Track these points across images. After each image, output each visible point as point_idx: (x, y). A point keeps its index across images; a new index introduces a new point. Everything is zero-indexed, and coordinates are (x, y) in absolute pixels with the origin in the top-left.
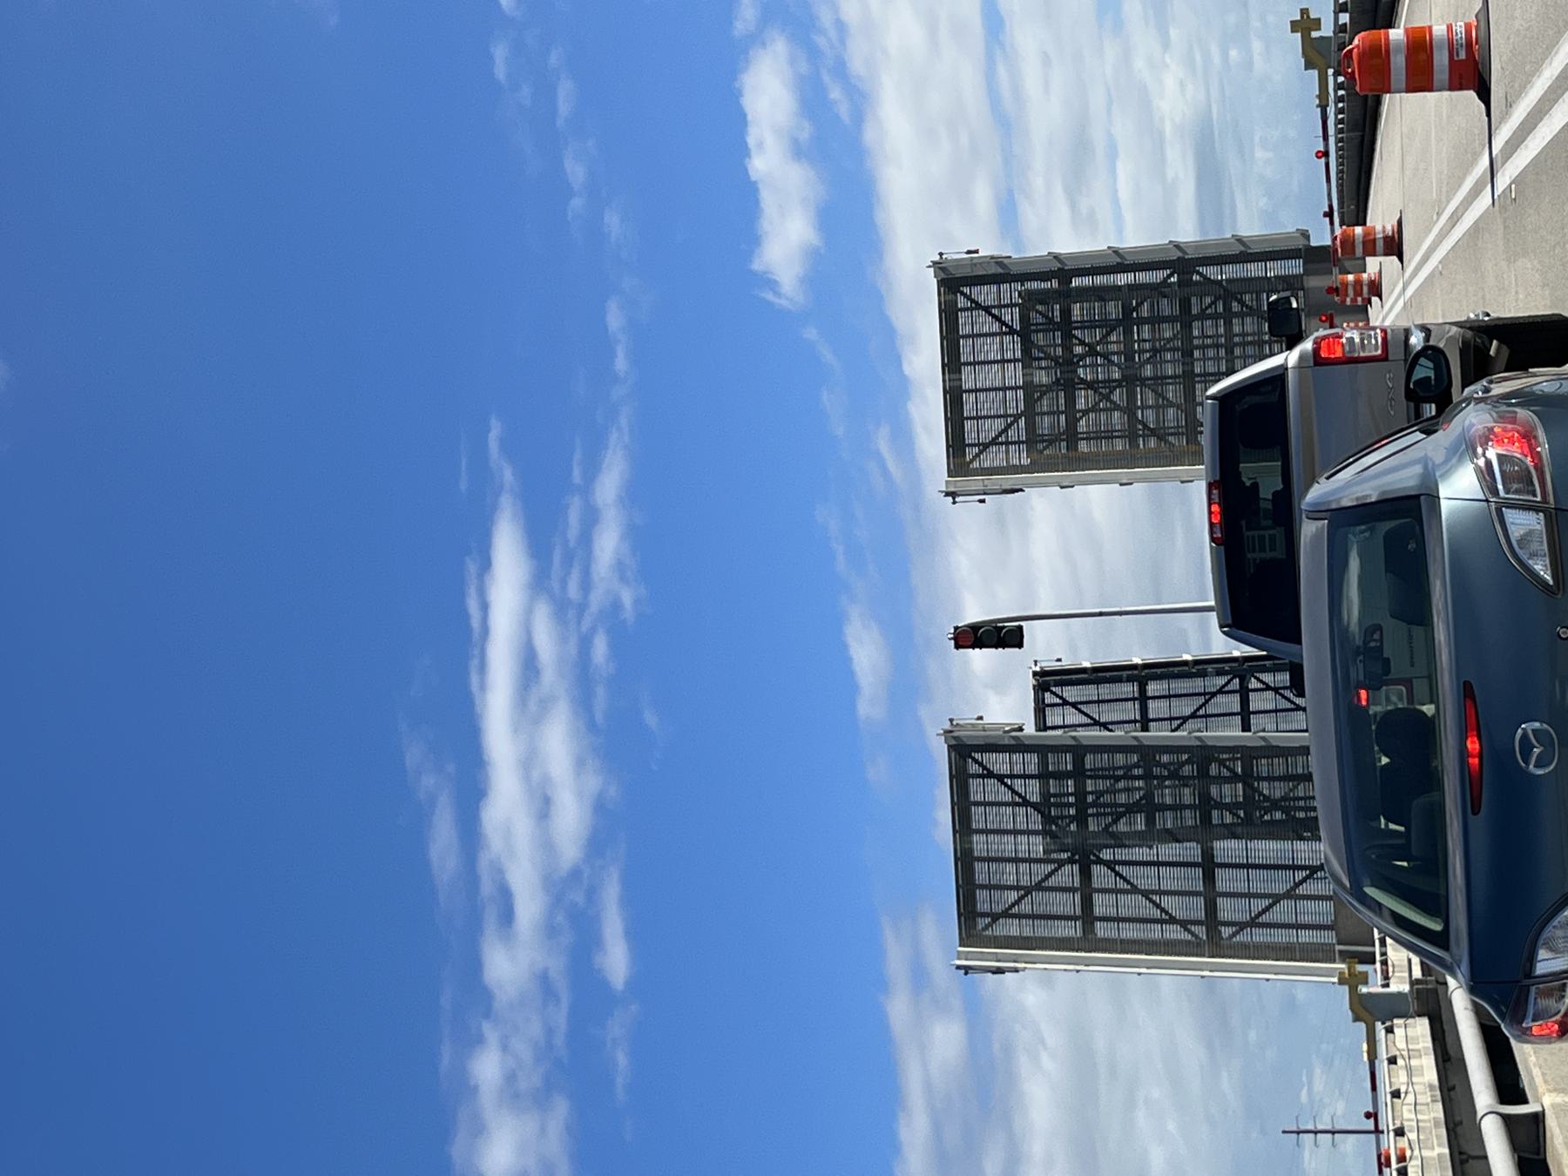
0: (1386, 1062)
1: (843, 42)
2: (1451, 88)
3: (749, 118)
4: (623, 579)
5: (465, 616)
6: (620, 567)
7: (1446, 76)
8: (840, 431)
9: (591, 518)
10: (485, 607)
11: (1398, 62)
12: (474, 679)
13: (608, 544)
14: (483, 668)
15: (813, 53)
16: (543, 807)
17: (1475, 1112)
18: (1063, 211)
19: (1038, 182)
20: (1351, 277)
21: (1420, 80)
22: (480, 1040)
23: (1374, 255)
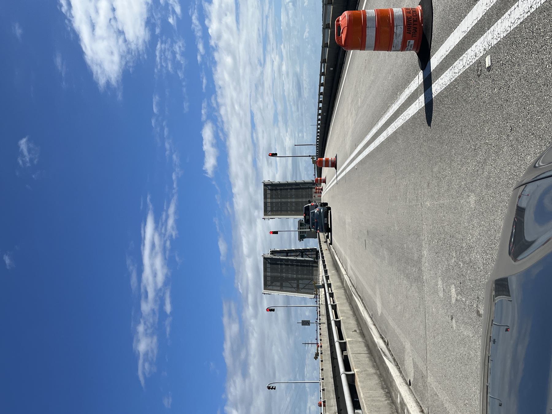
0: (319, 340)
1: (223, 125)
2: (332, 167)
3: (204, 138)
4: (173, 230)
5: (141, 234)
6: (173, 228)
7: (330, 165)
8: (219, 203)
9: (167, 217)
10: (145, 232)
11: (324, 163)
12: (142, 247)
13: (171, 222)
14: (144, 245)
15: (217, 127)
16: (155, 275)
17: (334, 342)
18: (266, 162)
19: (261, 157)
20: (318, 187)
21: (327, 166)
22: (140, 323)
23: (362, 46)
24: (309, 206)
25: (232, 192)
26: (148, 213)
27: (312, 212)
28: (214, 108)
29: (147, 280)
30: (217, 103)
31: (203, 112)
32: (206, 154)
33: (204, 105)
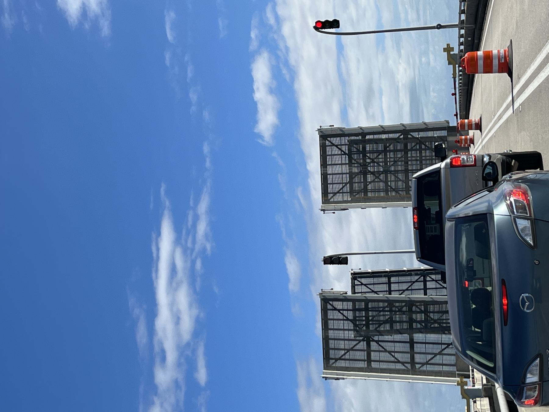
2: (499, 72)
3: (254, 79)
5: (151, 253)
6: (206, 236)
9: (196, 218)
10: (158, 249)
11: (481, 63)
13: (202, 227)
14: (157, 271)
15: (277, 57)
20: (463, 137)
21: (488, 69)
22: (153, 403)
24: (438, 172)
25: (307, 170)
26: (162, 214)
27: (460, 221)
28: (271, 27)
29: (164, 329)
30: (277, 18)
31: (253, 35)
32: (260, 107)
33: (254, 22)
